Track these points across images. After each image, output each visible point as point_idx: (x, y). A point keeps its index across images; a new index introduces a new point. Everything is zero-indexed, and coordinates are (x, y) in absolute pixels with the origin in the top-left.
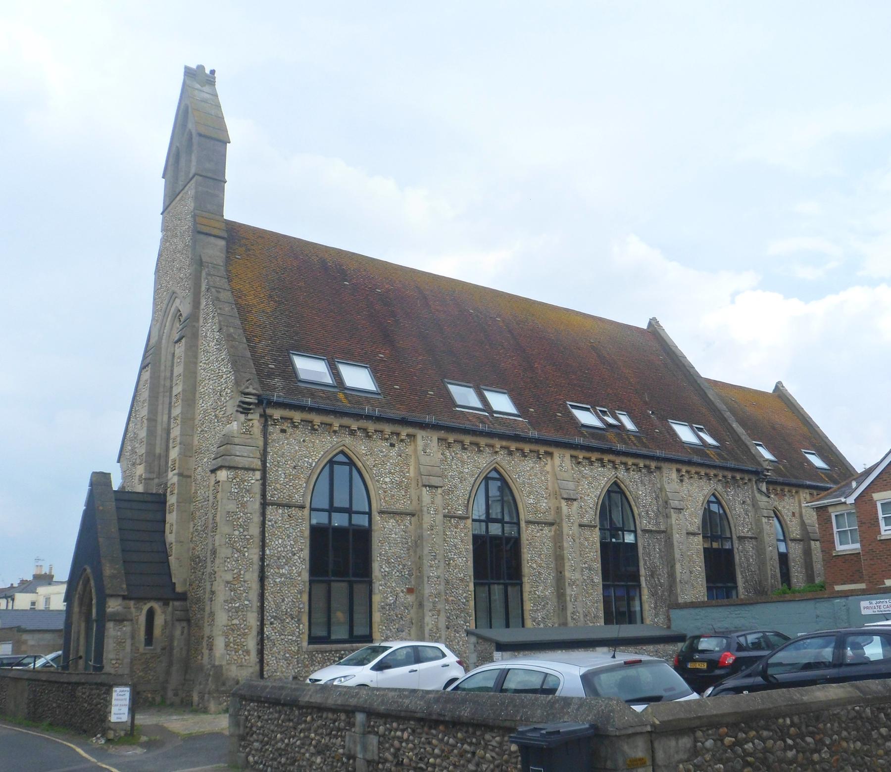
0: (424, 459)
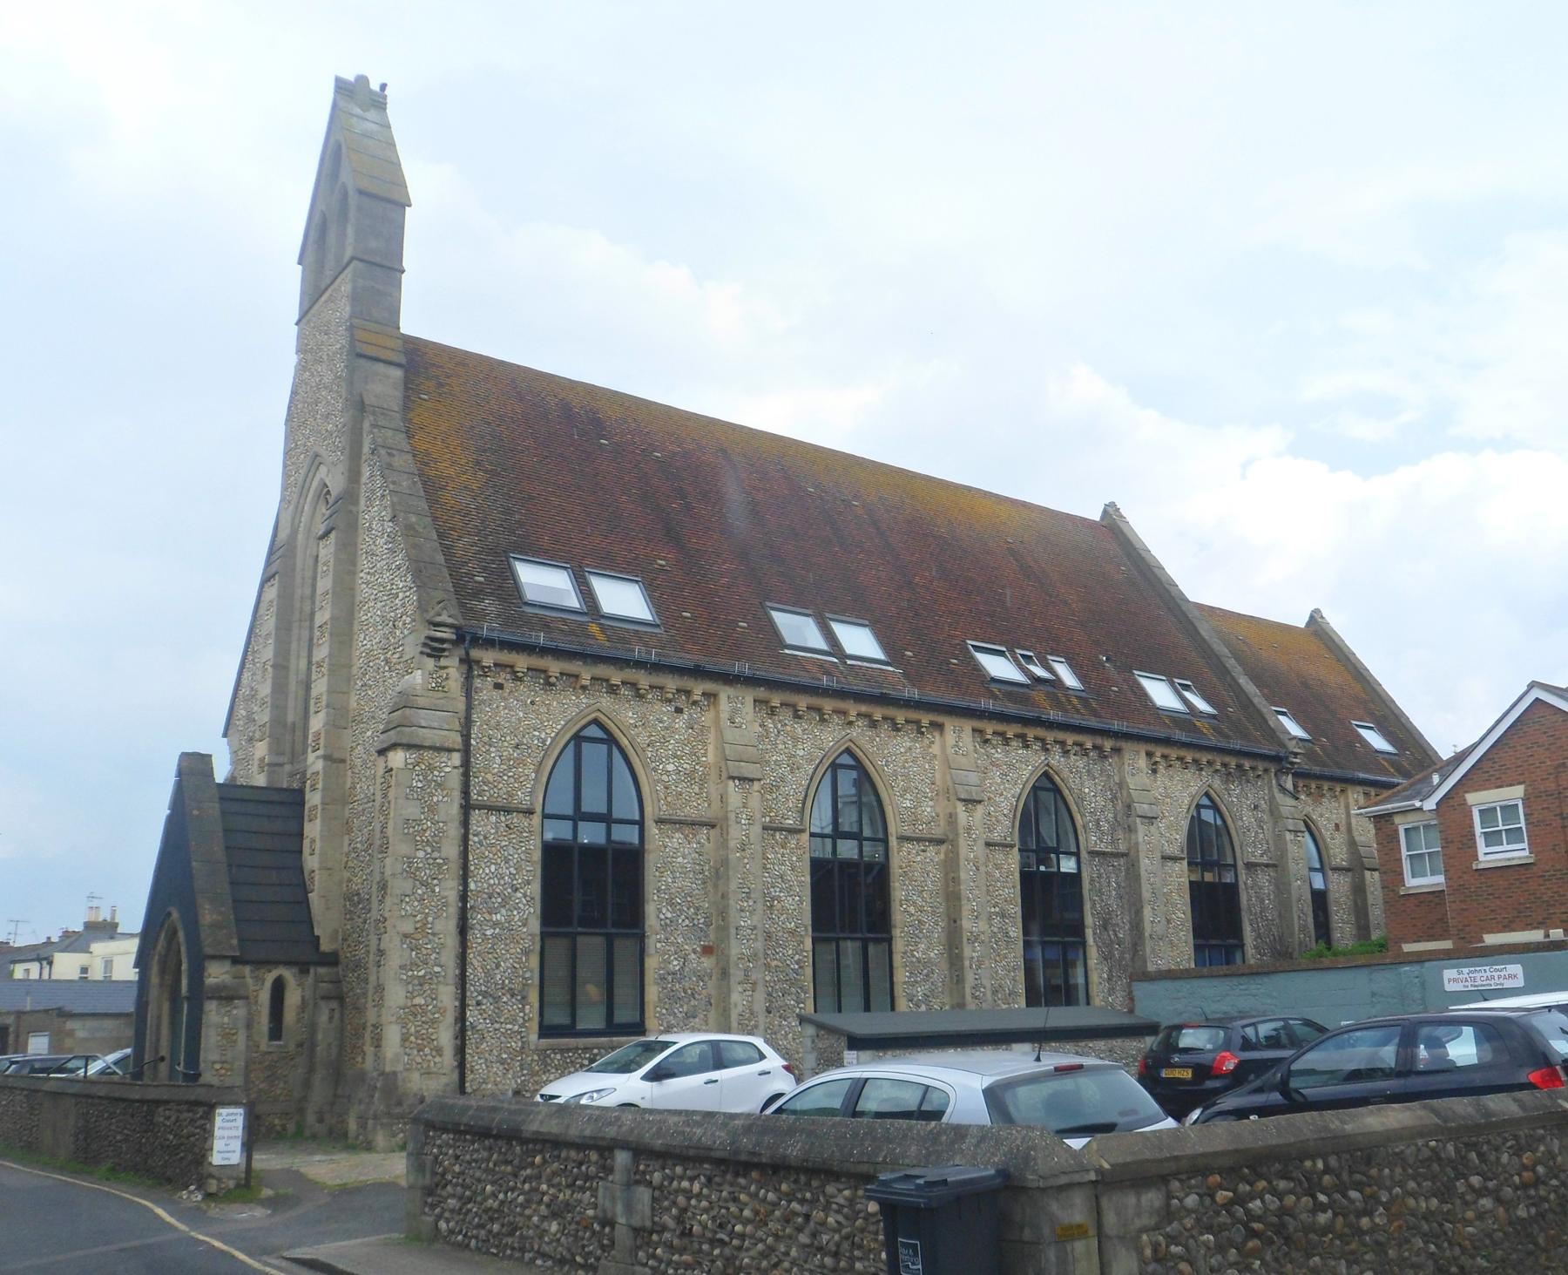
0: (730, 734)
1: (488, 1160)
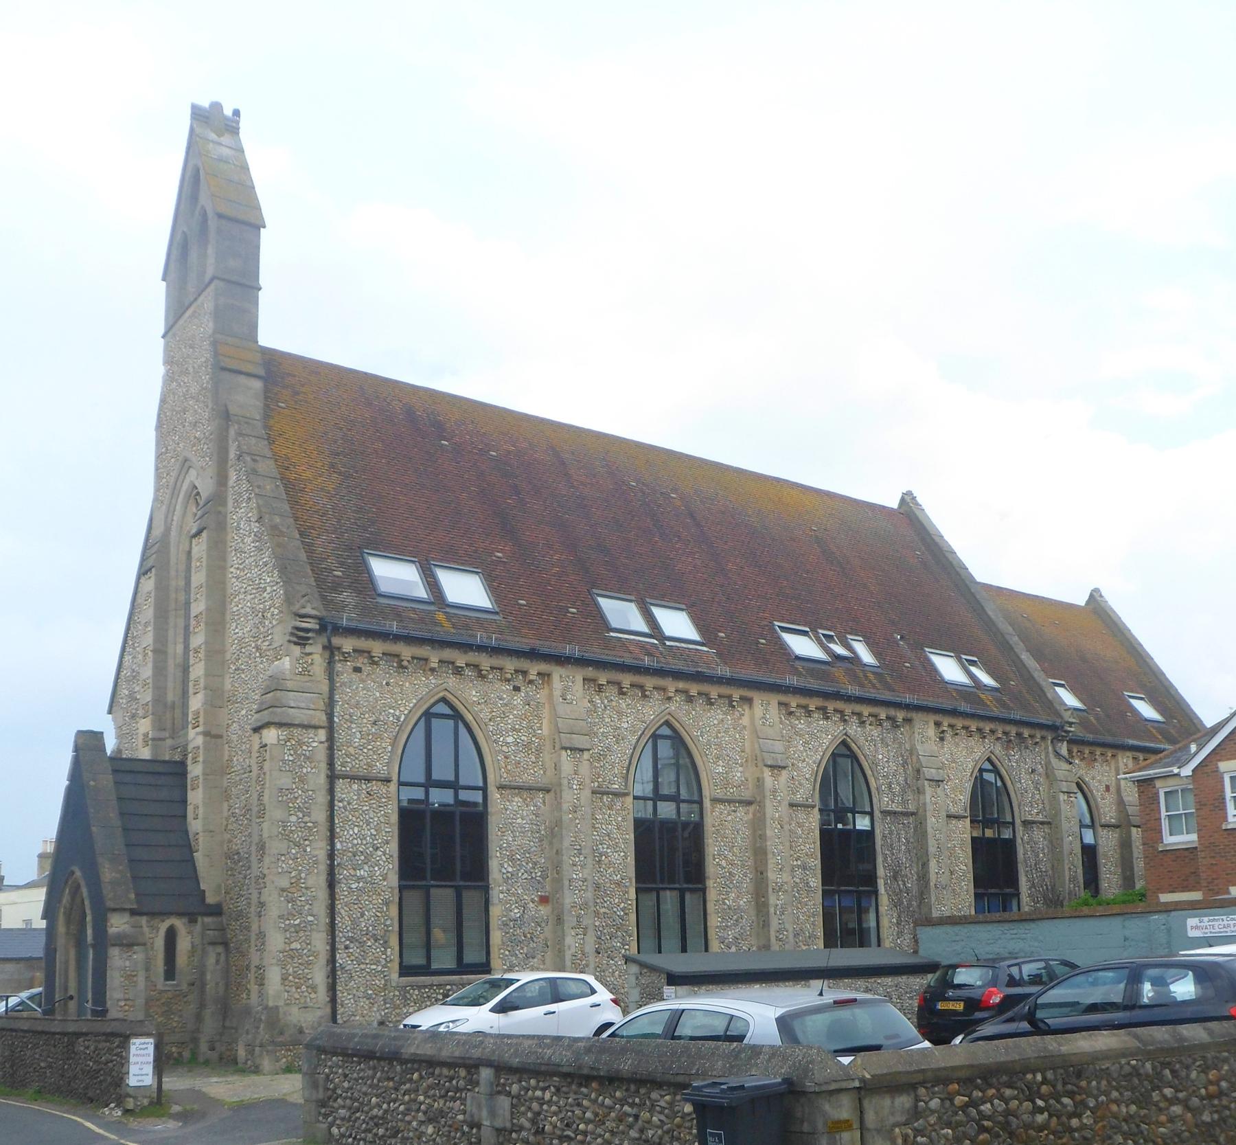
0: (562, 709)
1: (373, 1078)
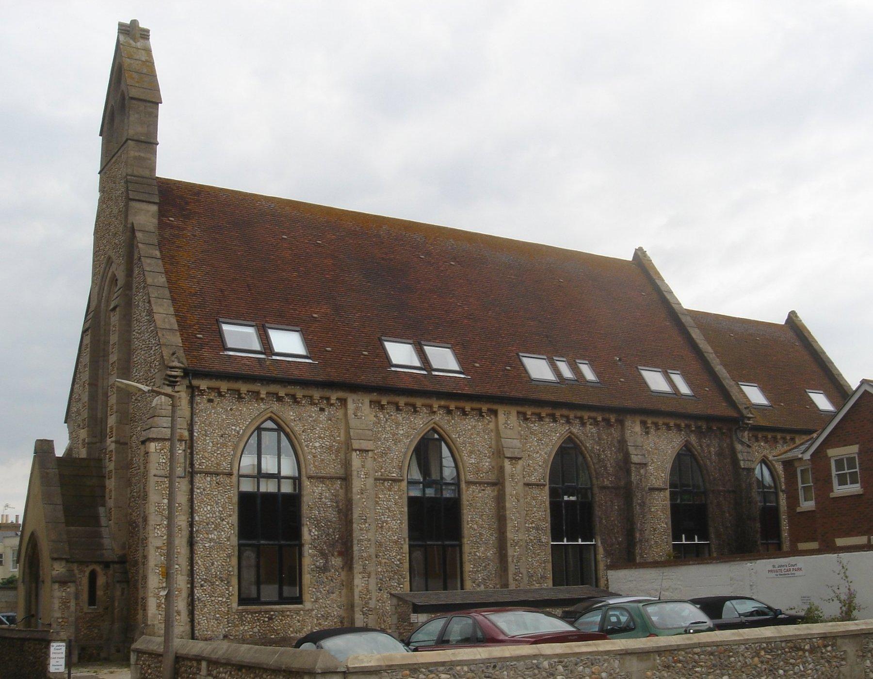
0: (353, 422)
